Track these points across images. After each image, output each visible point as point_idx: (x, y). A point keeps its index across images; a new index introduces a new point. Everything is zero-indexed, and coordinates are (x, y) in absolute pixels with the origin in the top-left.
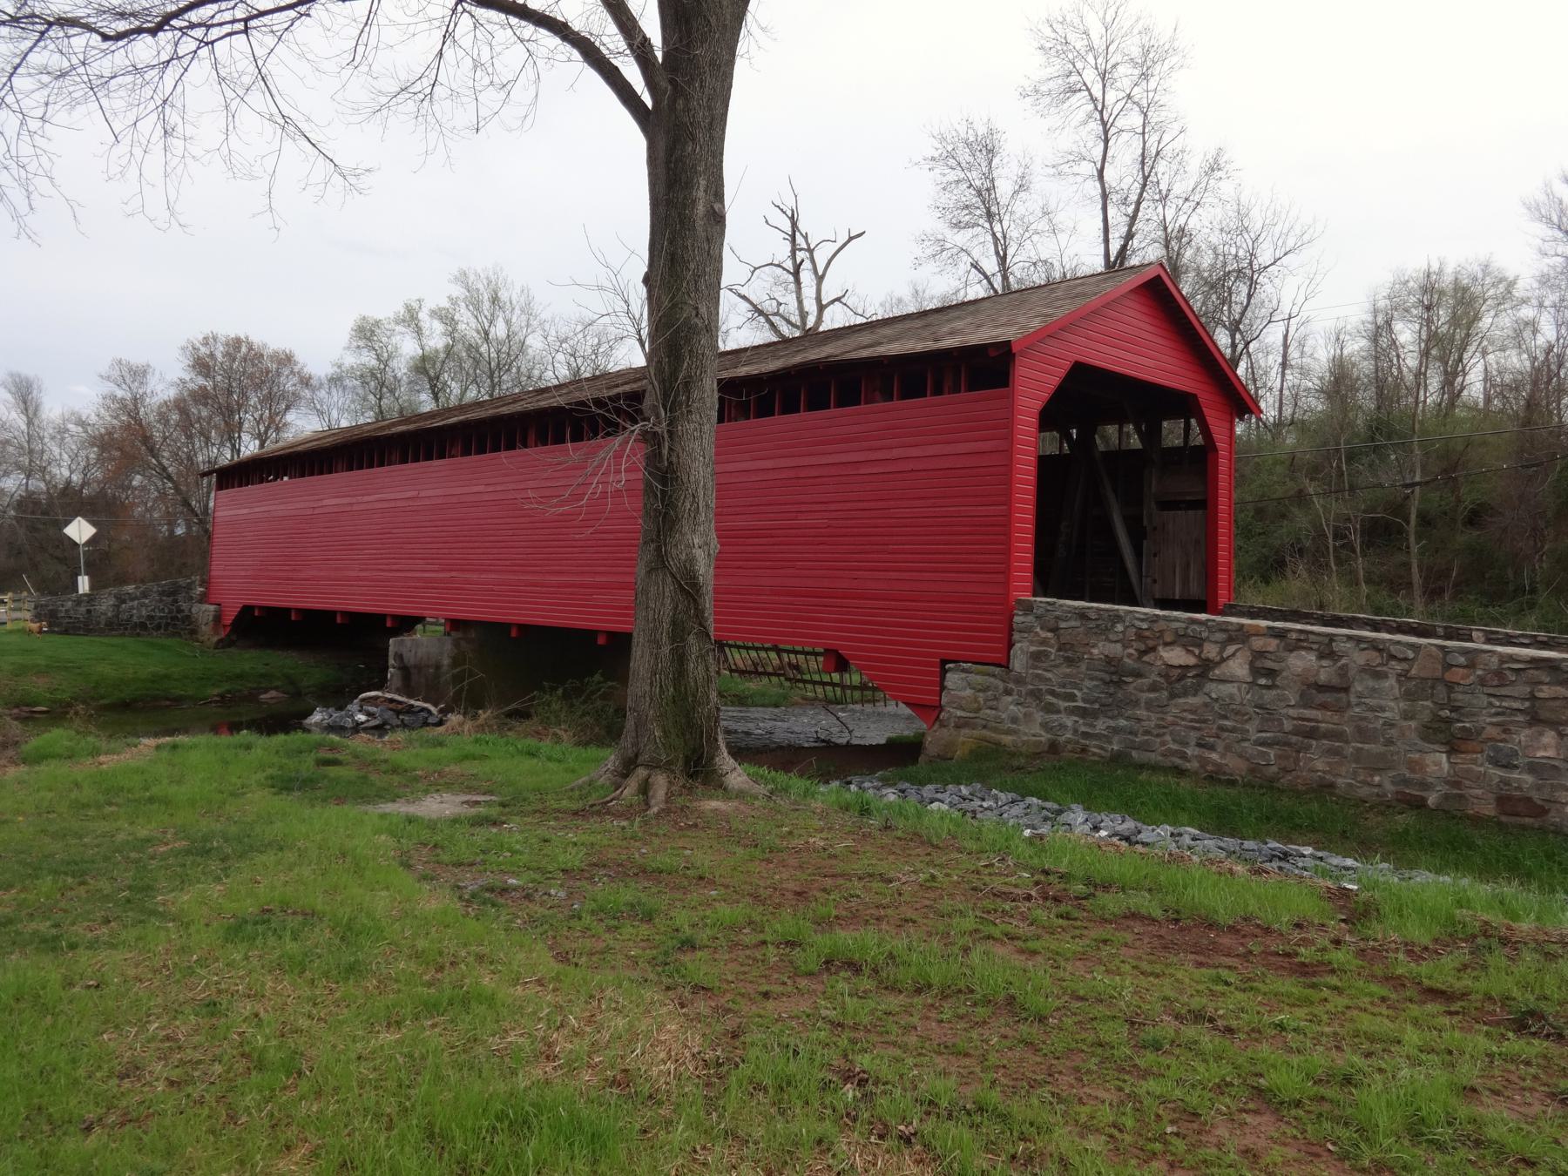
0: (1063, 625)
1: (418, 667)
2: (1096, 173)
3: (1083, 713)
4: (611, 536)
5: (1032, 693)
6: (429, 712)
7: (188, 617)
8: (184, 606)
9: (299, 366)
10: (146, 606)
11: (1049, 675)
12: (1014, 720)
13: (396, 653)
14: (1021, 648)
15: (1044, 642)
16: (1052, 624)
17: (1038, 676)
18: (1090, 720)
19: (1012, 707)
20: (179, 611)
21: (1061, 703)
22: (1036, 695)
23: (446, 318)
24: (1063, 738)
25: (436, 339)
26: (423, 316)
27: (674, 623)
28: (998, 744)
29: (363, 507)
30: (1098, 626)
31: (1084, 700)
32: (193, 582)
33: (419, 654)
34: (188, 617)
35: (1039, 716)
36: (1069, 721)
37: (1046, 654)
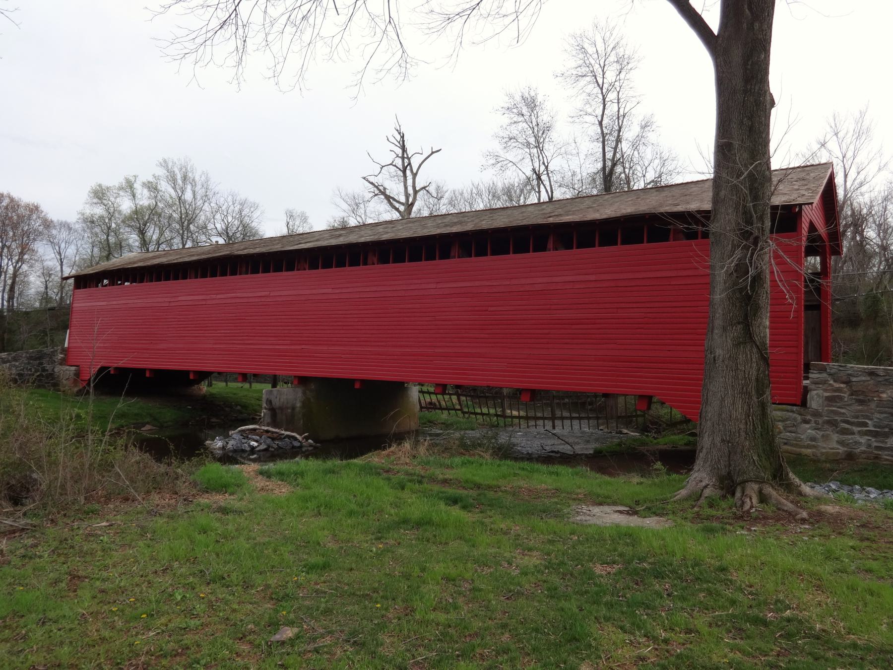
0: (854, 379)
1: (281, 408)
2: (597, 123)
3: (875, 434)
4: (450, 323)
5: (829, 422)
6: (295, 439)
7: (51, 375)
8: (48, 367)
9: (43, 214)
10: (16, 367)
11: (843, 411)
12: (813, 439)
13: (267, 400)
14: (817, 394)
15: (838, 390)
16: (845, 378)
17: (832, 411)
18: (881, 439)
19: (809, 431)
20: (44, 370)
21: (854, 428)
22: (832, 423)
23: (152, 187)
24: (858, 450)
25: (144, 199)
26: (137, 186)
27: (757, 380)
28: (800, 454)
29: (214, 302)
30: (886, 380)
31: (875, 426)
32: (57, 351)
33: (282, 400)
34: (51, 375)
35: (835, 437)
36: (863, 440)
37: (841, 398)
